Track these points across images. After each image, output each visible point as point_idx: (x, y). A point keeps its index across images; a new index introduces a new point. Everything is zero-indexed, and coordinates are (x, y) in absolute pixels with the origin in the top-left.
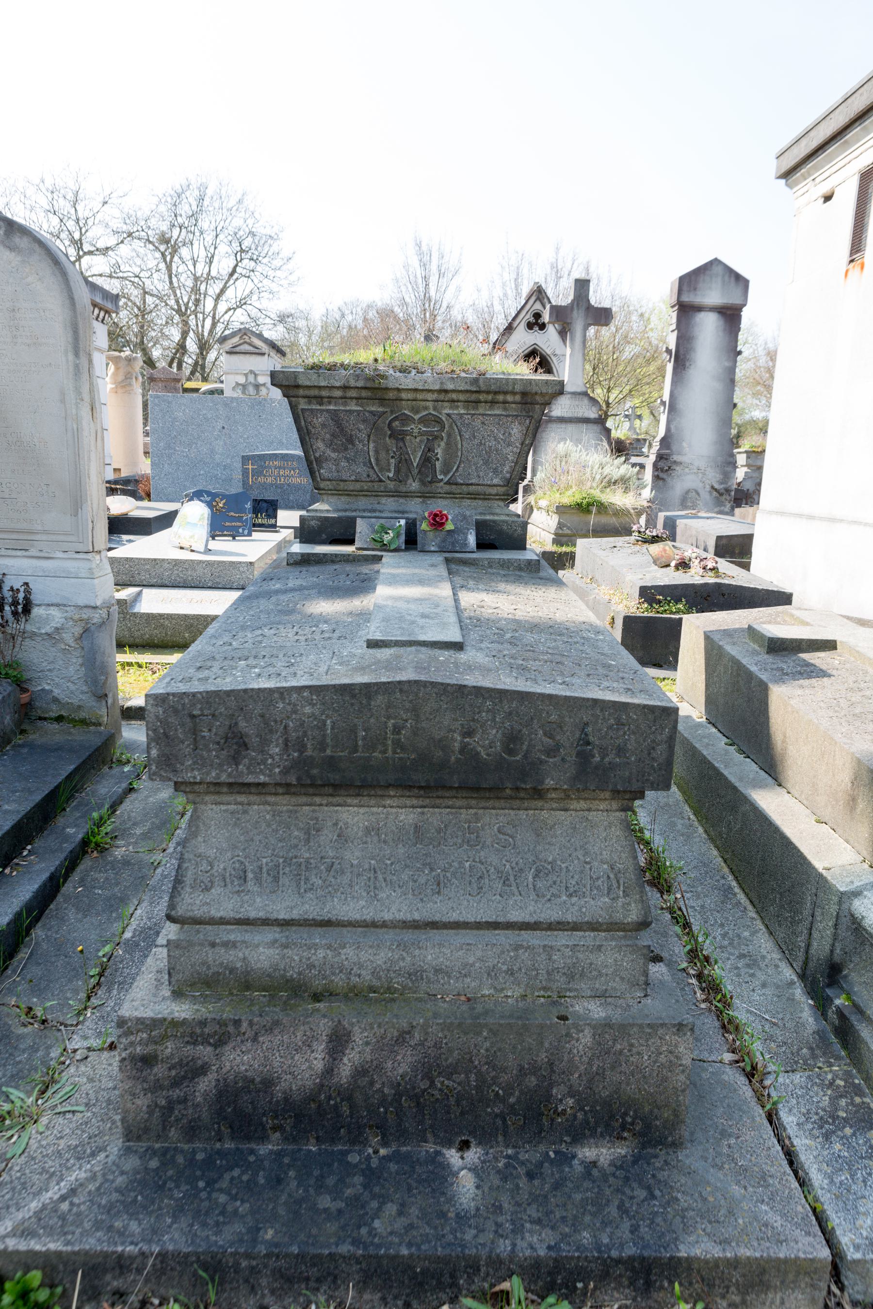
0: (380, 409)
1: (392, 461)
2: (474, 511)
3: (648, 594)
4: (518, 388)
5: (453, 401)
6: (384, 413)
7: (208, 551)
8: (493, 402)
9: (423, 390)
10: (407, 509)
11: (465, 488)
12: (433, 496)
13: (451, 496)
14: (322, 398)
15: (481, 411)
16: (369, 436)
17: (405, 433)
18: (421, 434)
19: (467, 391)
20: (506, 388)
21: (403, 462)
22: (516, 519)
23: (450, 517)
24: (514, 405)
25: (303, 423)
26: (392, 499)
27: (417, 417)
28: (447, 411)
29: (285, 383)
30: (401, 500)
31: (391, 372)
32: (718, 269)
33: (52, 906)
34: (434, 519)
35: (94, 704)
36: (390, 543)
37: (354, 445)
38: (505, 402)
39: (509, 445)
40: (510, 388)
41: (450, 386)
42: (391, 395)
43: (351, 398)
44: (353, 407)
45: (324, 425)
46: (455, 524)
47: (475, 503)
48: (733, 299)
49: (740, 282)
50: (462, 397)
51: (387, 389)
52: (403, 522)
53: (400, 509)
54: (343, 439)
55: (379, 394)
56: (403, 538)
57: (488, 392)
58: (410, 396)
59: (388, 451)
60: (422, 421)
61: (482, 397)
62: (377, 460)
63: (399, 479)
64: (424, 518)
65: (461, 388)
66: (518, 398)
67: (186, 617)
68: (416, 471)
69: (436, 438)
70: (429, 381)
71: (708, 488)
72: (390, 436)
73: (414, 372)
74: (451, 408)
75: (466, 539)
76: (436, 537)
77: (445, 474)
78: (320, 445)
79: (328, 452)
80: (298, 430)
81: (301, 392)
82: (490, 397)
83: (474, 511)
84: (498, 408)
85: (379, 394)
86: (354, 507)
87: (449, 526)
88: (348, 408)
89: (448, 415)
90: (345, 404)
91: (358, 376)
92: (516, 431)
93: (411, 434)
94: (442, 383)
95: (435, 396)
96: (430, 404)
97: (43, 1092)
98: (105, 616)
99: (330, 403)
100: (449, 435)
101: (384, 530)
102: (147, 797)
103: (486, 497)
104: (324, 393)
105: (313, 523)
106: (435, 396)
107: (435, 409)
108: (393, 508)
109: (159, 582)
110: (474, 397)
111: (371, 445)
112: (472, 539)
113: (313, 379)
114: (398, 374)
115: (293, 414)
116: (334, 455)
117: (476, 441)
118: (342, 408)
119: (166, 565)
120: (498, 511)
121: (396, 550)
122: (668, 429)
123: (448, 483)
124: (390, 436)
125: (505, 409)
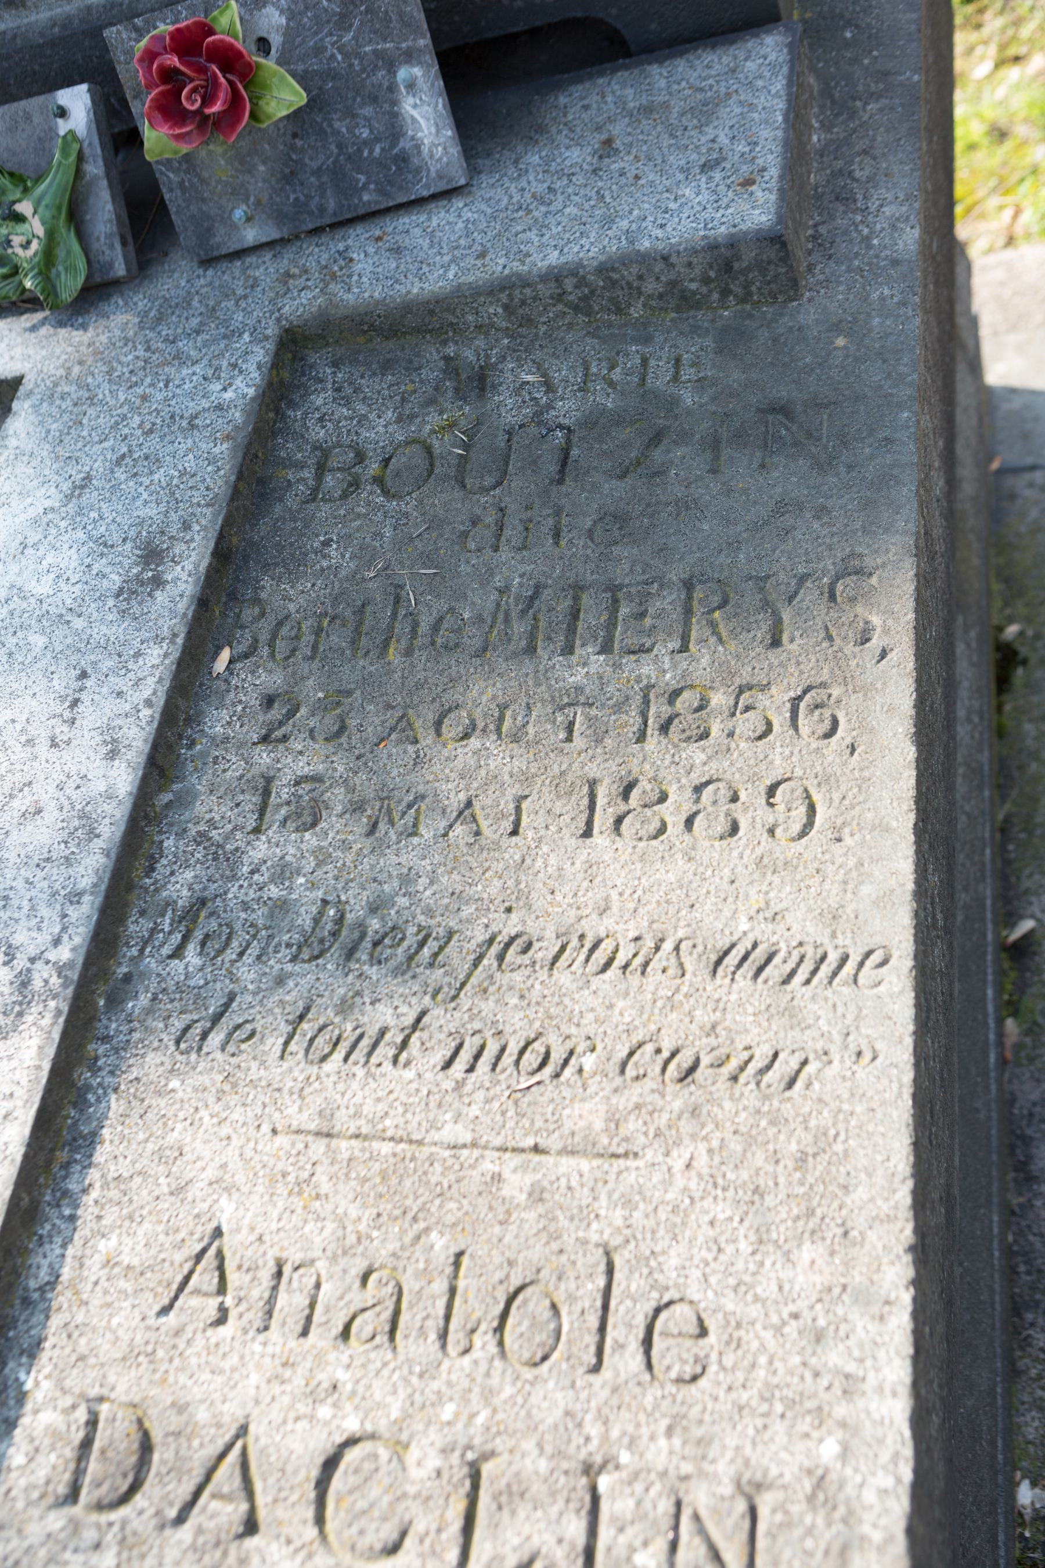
52: (77, 102)
75: (394, 127)
87: (283, 96)
112: (425, 116)
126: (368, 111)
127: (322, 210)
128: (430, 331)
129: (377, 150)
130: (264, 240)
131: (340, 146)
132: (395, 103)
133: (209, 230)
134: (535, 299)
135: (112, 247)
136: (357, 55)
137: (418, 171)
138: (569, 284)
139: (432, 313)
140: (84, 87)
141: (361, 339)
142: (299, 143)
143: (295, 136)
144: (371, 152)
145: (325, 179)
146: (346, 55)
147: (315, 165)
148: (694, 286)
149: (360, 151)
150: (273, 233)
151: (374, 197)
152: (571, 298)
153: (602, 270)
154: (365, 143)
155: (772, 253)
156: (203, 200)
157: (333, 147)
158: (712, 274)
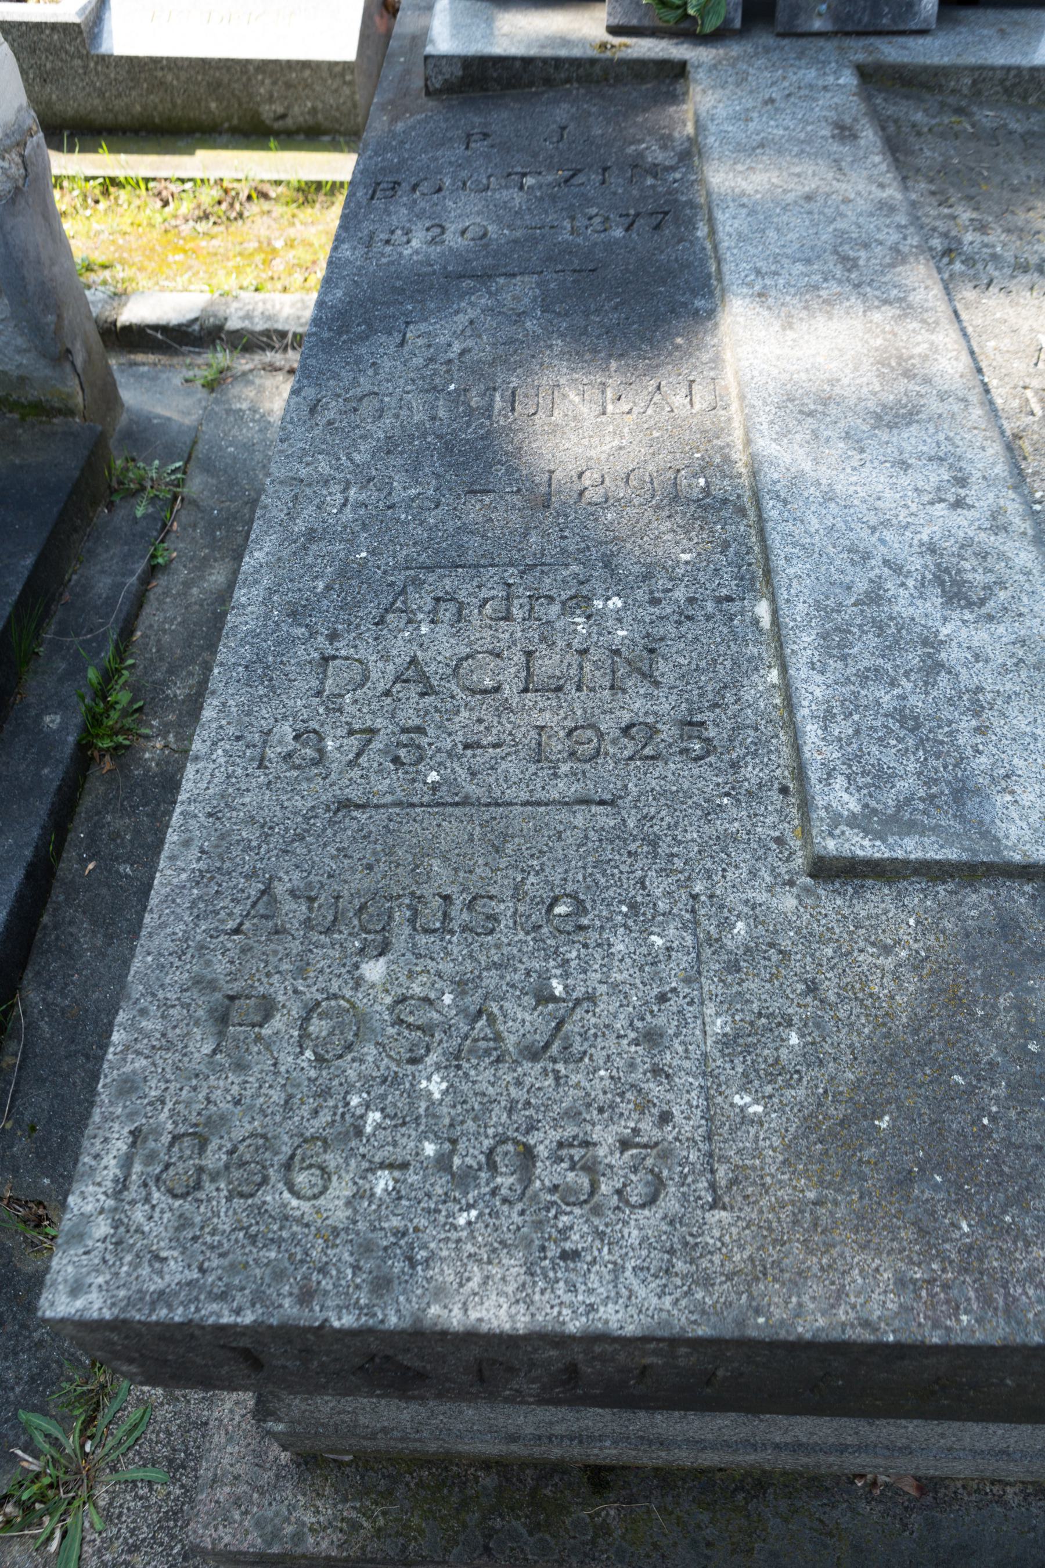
33: (45, 919)
35: (48, 372)
67: (204, 64)
97: (90, 1421)
98: (17, 171)
102: (188, 584)
127: (860, 21)
130: (823, 29)
135: (736, 10)
137: (916, 14)
138: (1013, 73)
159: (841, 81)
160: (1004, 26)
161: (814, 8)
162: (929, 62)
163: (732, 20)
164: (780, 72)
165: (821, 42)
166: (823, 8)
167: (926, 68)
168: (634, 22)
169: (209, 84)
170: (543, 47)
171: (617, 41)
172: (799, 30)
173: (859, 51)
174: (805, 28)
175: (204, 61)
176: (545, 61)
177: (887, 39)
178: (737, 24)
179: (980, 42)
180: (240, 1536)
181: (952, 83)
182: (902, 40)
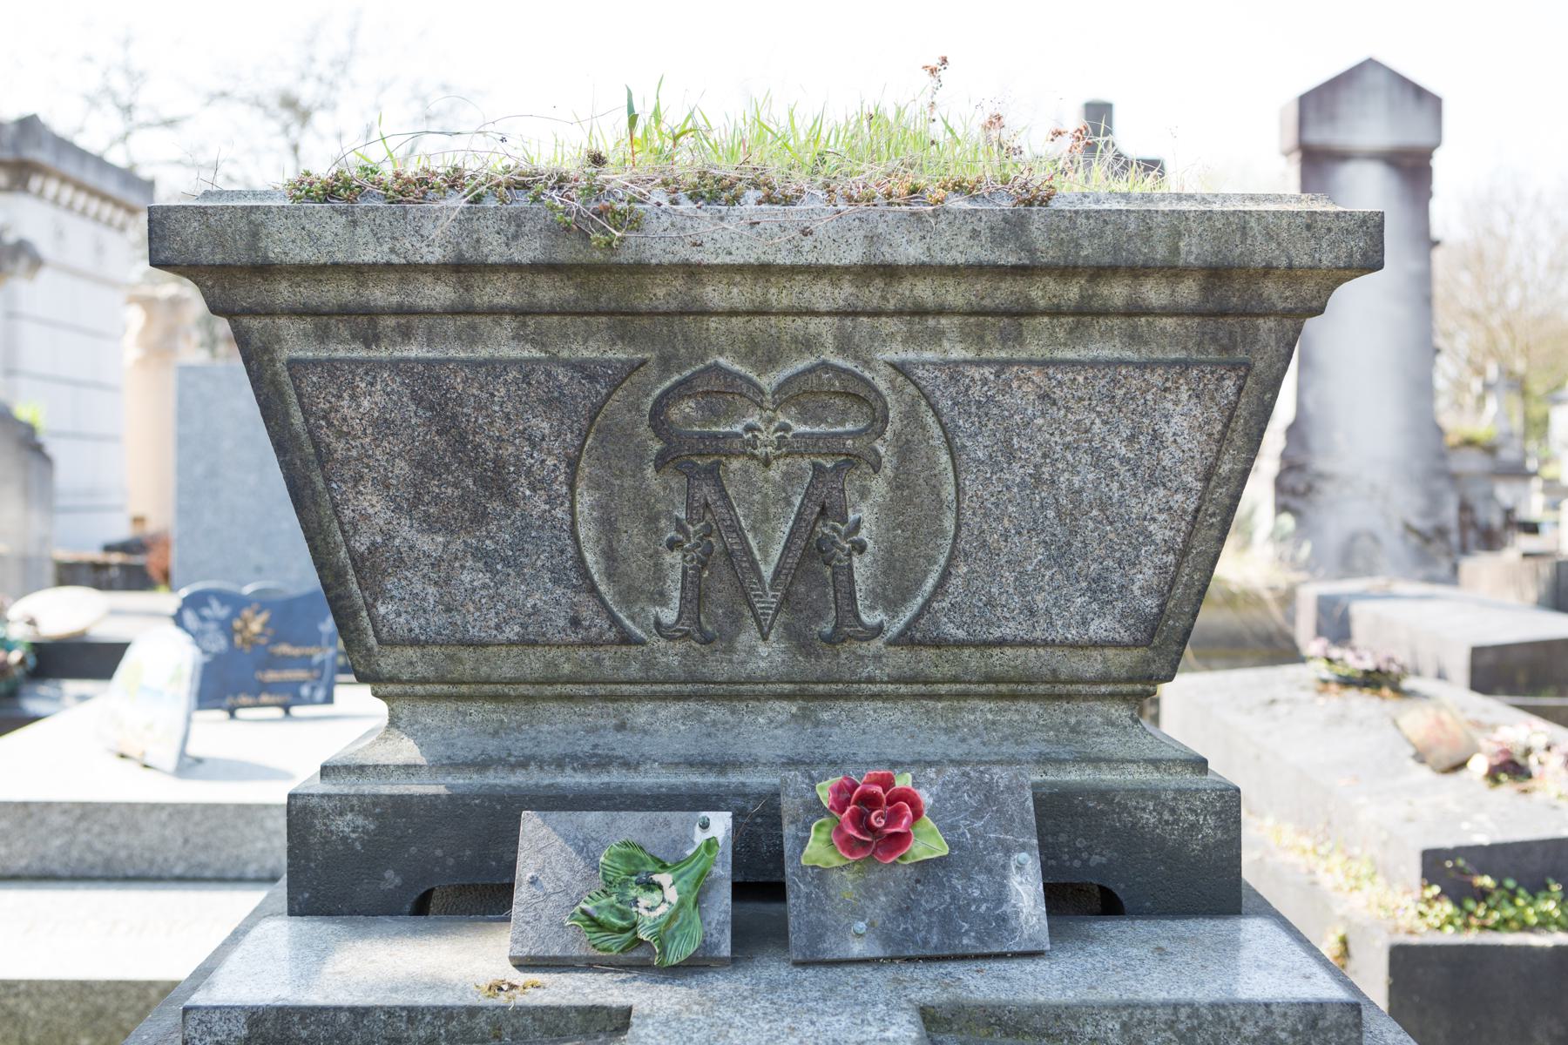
0: (619, 354)
1: (674, 559)
2: (1017, 753)
3: (1448, 872)
4: (1192, 250)
5: (920, 312)
6: (644, 362)
7: (189, 765)
8: (1086, 313)
9: (792, 271)
10: (738, 749)
11: (973, 659)
12: (846, 691)
13: (917, 688)
14: (372, 313)
15: (1035, 348)
16: (573, 464)
17: (721, 447)
18: (789, 447)
19: (978, 269)
20: (1141, 252)
21: (718, 564)
22: (1188, 779)
23: (925, 798)
24: (1169, 323)
25: (297, 418)
26: (675, 708)
27: (768, 381)
28: (895, 353)
29: (209, 255)
30: (715, 712)
31: (659, 196)
32: (1373, 78)
34: (860, 821)
36: (663, 936)
37: (510, 501)
38: (1134, 311)
39: (1152, 483)
40: (1161, 252)
41: (909, 251)
42: (660, 294)
43: (495, 312)
44: (503, 345)
45: (383, 426)
46: (948, 829)
47: (1012, 714)
48: (1410, 134)
49: (1424, 99)
50: (955, 294)
51: (641, 269)
52: (720, 824)
53: (711, 748)
54: (464, 474)
55: (610, 293)
56: (722, 901)
57: (1066, 271)
58: (740, 294)
59: (653, 519)
60: (793, 394)
61: (1040, 292)
62: (610, 556)
63: (704, 627)
64: (815, 808)
65: (955, 257)
66: (1188, 292)
68: (772, 598)
69: (851, 461)
70: (819, 227)
71: (1397, 528)
72: (661, 462)
73: (752, 195)
74: (910, 339)
75: (1001, 896)
76: (869, 892)
77: (892, 606)
78: (371, 502)
79: (406, 531)
80: (280, 447)
81: (284, 292)
82: (1072, 292)
83: (1017, 753)
84: (1106, 335)
85: (610, 293)
86: (521, 745)
87: (928, 843)
88: (483, 353)
89: (900, 368)
90: (471, 337)
91: (517, 219)
92: (1183, 422)
93: (747, 449)
94: (871, 239)
95: (844, 293)
96: (823, 328)
99: (406, 334)
100: (905, 451)
101: (640, 870)
103: (1056, 690)
104: (380, 294)
105: (343, 824)
106: (844, 293)
107: (844, 345)
108: (679, 748)
109: (36, 867)
110: (1005, 292)
111: (585, 500)
112: (1025, 893)
113: (333, 238)
114: (686, 206)
115: (256, 380)
116: (429, 544)
117: (1018, 472)
118: (458, 352)
119: (56, 819)
120: (1109, 744)
121: (696, 966)
122: (1300, 406)
123: (905, 640)
124: (661, 462)
125: (1134, 338)
126: (982, 878)
127: (926, 942)
128: (1048, 1036)
129: (984, 908)
130: (868, 955)
131: (953, 898)
132: (1005, 877)
133: (820, 936)
134: (1150, 1021)
136: (983, 837)
137: (1013, 930)
138: (1183, 1013)
139: (1058, 1017)
140: (730, 814)
141: (983, 1032)
142: (920, 888)
143: (918, 881)
144: (978, 907)
145: (934, 919)
146: (974, 836)
147: (928, 906)
148: (1283, 1035)
149: (969, 905)
150: (877, 951)
151: (973, 942)
152: (1181, 1027)
153: (1213, 1006)
154: (974, 900)
155: (1349, 1018)
156: (824, 912)
157: (947, 897)
158: (1300, 1027)
159: (890, 1034)
160: (1163, 944)
161: (848, 926)
162: (1041, 999)
163: (717, 946)
164: (788, 1020)
165: (867, 972)
166: (861, 926)
167: (1038, 1009)
168: (556, 951)
169: (85, 1014)
170: (395, 990)
171: (520, 978)
172: (828, 957)
173: (928, 985)
174: (838, 954)
175: (84, 985)
176: (390, 1012)
177: (973, 966)
178: (725, 950)
179: (1127, 966)
180: (1561, 904)
181: (1089, 1029)
182: (997, 966)
